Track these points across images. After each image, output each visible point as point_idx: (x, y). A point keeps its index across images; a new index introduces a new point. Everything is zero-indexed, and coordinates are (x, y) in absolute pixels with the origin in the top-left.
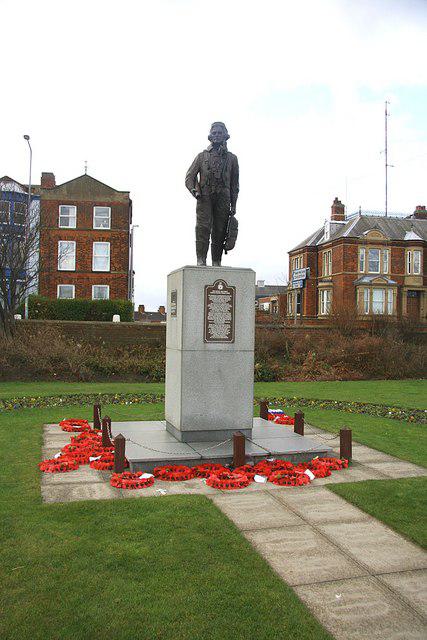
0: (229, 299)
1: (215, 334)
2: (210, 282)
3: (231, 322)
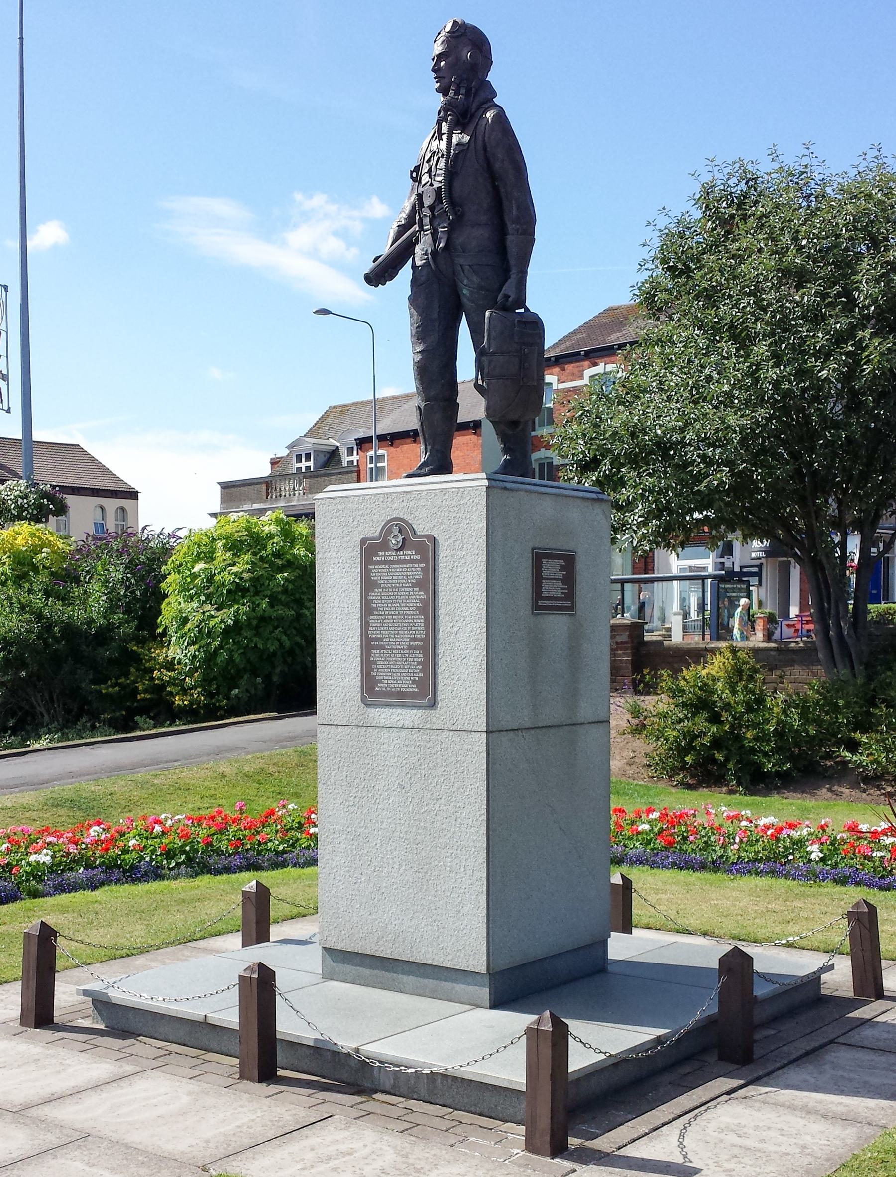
0: (419, 576)
1: (387, 680)
2: (373, 531)
3: (425, 640)
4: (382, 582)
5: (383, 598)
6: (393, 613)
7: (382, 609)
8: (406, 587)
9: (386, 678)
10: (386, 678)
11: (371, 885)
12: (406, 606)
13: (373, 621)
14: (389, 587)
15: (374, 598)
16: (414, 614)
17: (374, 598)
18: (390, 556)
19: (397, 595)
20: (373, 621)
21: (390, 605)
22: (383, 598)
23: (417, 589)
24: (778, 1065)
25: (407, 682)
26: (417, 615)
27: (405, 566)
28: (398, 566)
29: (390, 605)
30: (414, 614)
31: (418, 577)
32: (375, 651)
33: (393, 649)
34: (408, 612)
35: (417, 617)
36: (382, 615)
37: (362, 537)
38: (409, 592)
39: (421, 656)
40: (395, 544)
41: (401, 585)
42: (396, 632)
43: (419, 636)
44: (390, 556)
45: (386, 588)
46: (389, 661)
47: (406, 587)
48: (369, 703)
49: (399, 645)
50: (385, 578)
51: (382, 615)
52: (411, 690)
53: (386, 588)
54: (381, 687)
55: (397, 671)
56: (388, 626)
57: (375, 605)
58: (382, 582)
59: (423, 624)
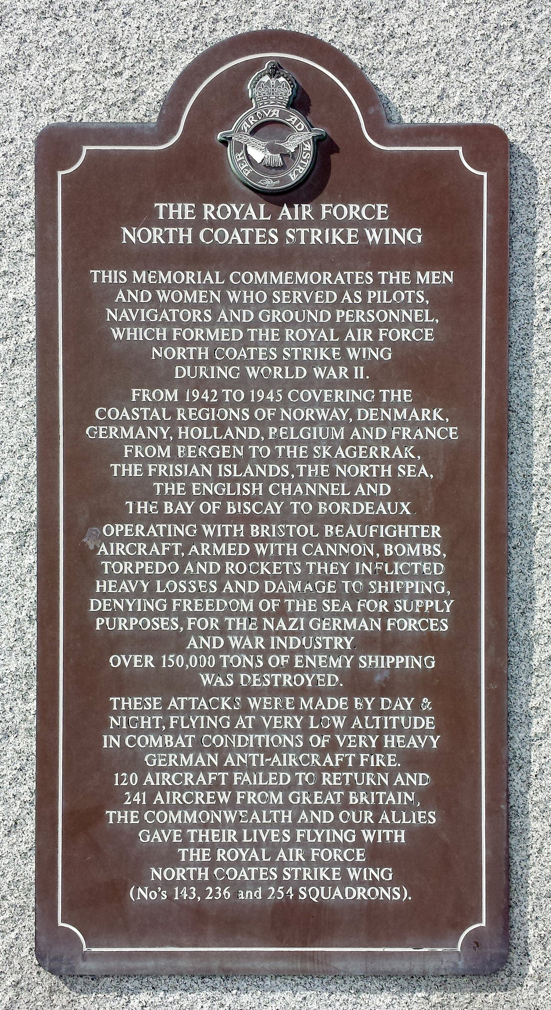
4: (180, 353)
5: (184, 433)
6: (249, 509)
7: (179, 489)
8: (331, 384)
9: (204, 835)
10: (204, 835)
11: (435, 50)
12: (333, 477)
13: (121, 549)
14: (221, 383)
15: (128, 433)
16: (380, 520)
17: (128, 433)
18: (231, 224)
19: (276, 421)
20: (121, 549)
21: (230, 471)
22: (184, 433)
23: (405, 395)
24: (311, 177)
25: (335, 854)
26: (403, 520)
27: (326, 277)
28: (168, 277)
29: (230, 471)
30: (380, 520)
31: (404, 335)
32: (134, 703)
33: (249, 691)
34: (343, 508)
35: (402, 531)
36: (179, 519)
37: (45, 121)
38: (352, 407)
39: (428, 722)
40: (268, 168)
41: (301, 372)
42: (272, 604)
43: (411, 625)
44: (231, 224)
45: (201, 384)
46: (222, 753)
47: (331, 384)
48: (91, 966)
49: (290, 668)
50: (197, 334)
51: (179, 519)
52: (361, 893)
53: (201, 384)
54: (168, 885)
55: (277, 798)
56: (221, 578)
57: (134, 470)
58: (180, 353)
59: (438, 568)
